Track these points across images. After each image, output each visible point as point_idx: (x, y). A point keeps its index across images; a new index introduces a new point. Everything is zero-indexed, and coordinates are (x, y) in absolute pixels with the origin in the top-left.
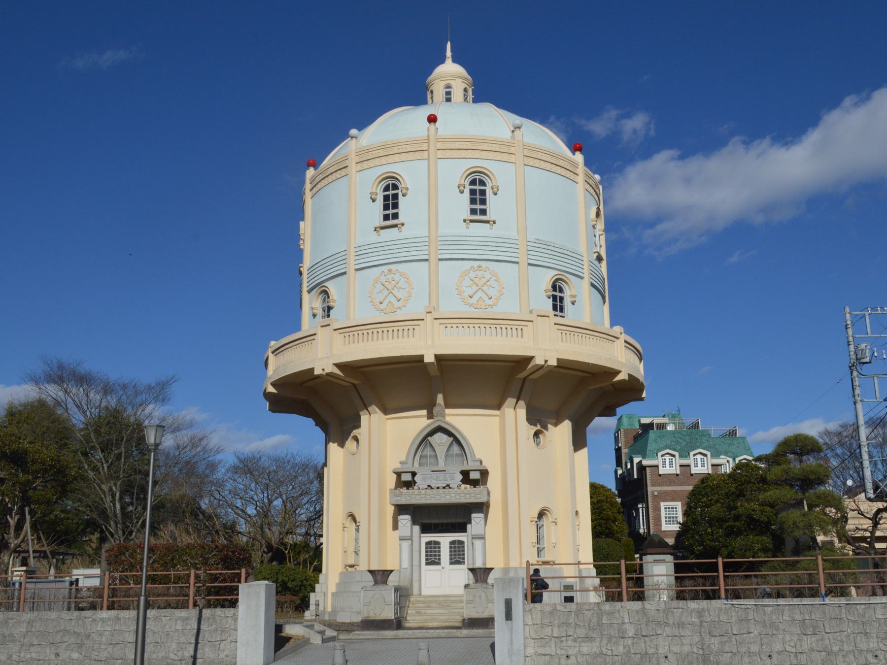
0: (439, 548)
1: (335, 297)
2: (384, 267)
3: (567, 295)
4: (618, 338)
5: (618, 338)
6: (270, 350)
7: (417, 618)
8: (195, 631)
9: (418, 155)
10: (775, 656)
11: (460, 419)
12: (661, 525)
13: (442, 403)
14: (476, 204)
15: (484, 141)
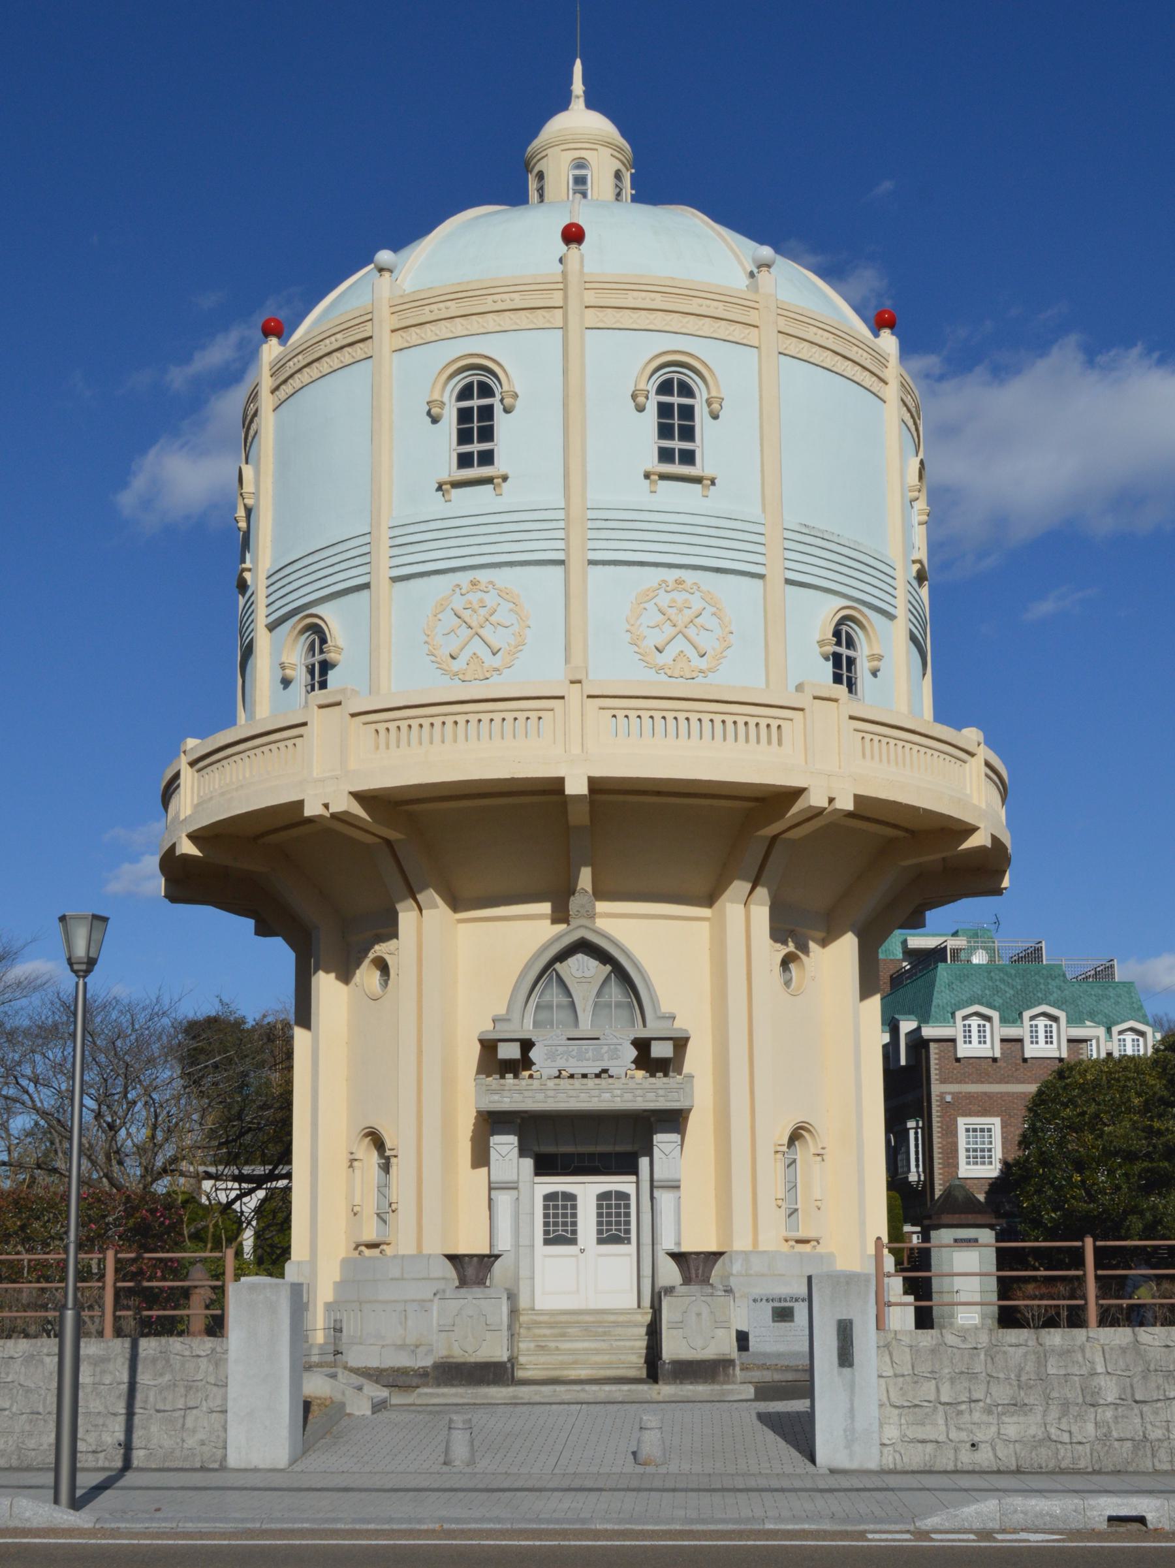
0: (574, 1207)
1: (341, 642)
2: (459, 575)
3: (863, 654)
4: (972, 755)
5: (972, 755)
6: (184, 761)
7: (542, 1359)
8: (124, 1387)
9: (540, 318)
11: (625, 924)
12: (956, 1166)
13: (589, 889)
14: (672, 438)
15: (692, 293)
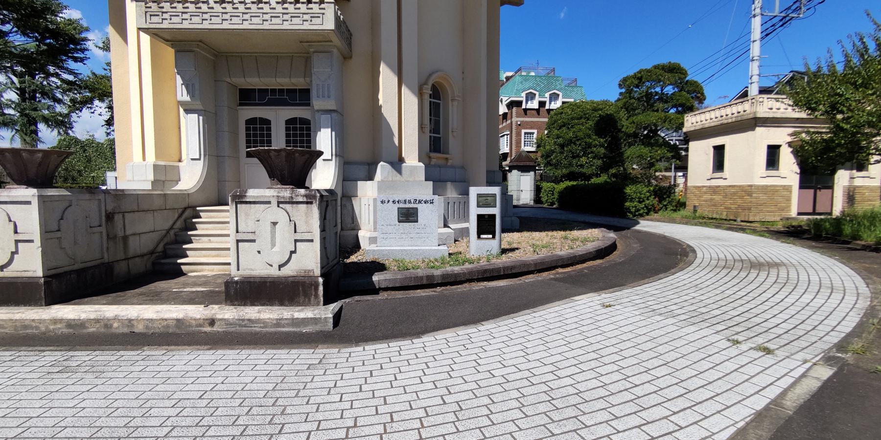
0: (269, 129)
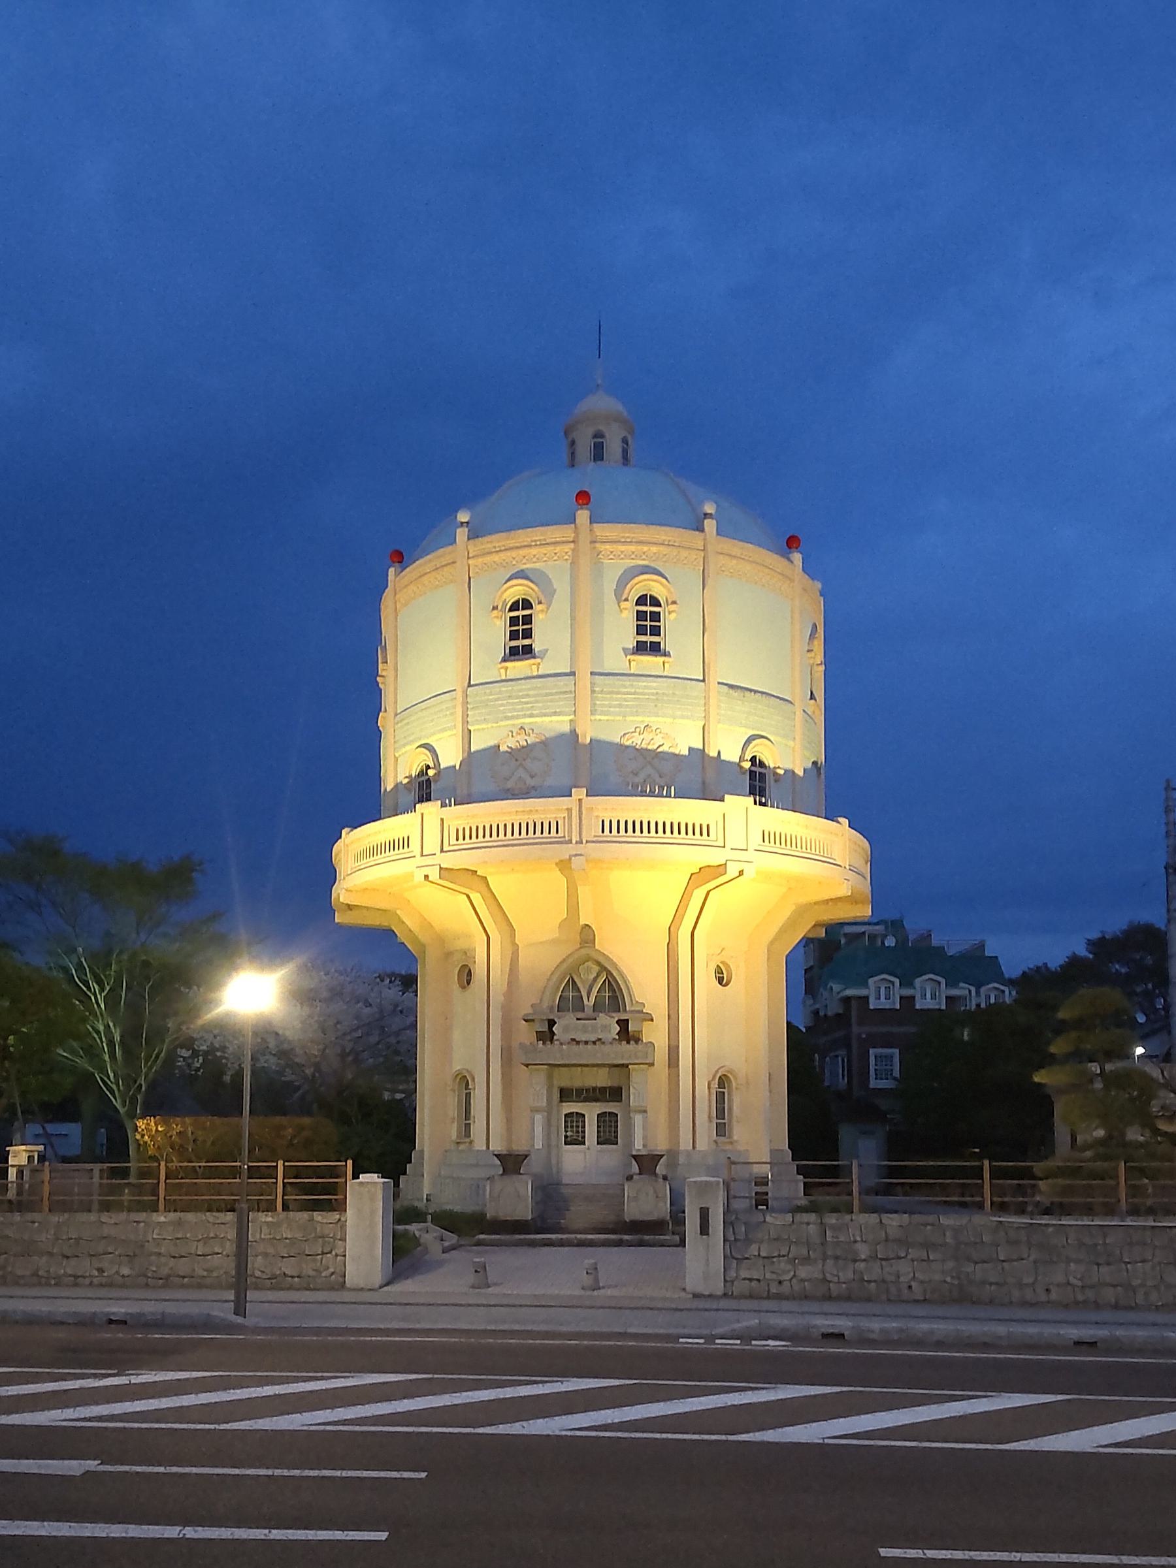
10: (1054, 1290)
